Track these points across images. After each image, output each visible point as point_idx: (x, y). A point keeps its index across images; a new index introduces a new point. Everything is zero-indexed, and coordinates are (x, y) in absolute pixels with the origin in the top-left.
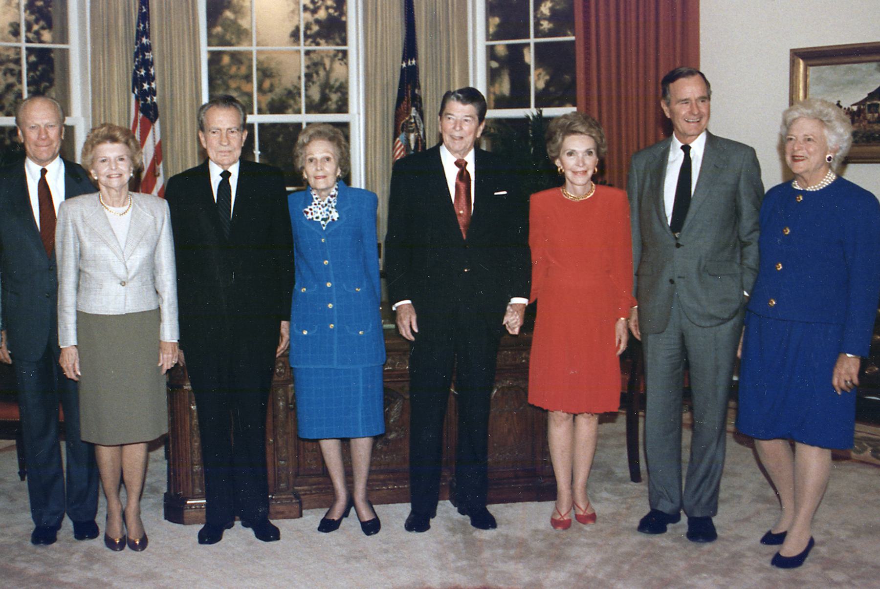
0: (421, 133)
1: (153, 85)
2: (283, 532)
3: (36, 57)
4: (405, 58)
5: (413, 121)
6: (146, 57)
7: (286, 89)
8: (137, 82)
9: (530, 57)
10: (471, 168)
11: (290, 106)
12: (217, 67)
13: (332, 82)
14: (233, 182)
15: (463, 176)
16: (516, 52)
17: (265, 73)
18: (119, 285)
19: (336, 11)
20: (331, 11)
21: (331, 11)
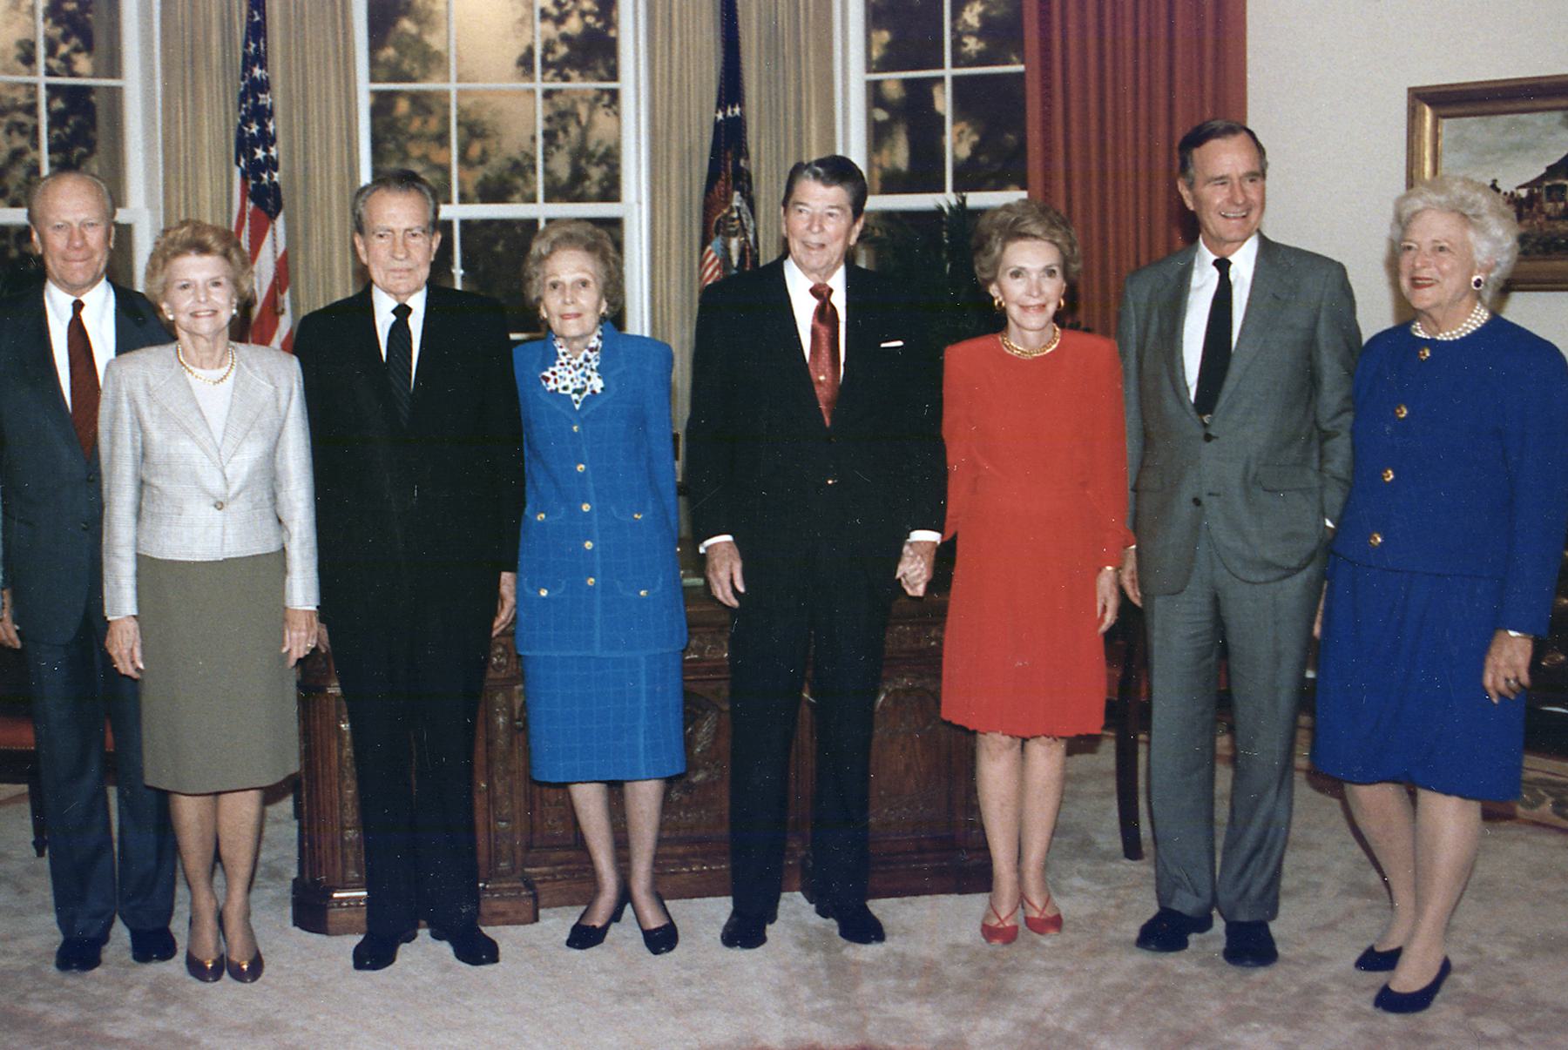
0: (751, 237)
1: (273, 151)
2: (504, 948)
3: (64, 101)
4: (722, 104)
5: (735, 215)
6: (261, 102)
7: (509, 159)
8: (244, 145)
9: (944, 102)
10: (839, 300)
11: (517, 189)
12: (387, 119)
13: (591, 146)
14: (416, 324)
15: (825, 313)
16: (920, 92)
17: (473, 130)
18: (212, 509)
19: (598, 20)
20: (590, 19)
21: (590, 19)
